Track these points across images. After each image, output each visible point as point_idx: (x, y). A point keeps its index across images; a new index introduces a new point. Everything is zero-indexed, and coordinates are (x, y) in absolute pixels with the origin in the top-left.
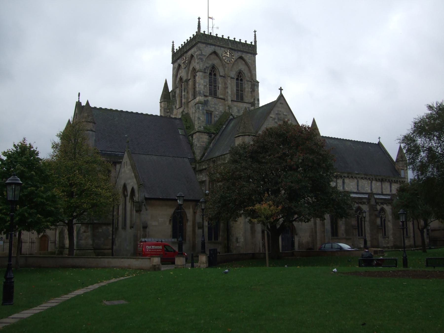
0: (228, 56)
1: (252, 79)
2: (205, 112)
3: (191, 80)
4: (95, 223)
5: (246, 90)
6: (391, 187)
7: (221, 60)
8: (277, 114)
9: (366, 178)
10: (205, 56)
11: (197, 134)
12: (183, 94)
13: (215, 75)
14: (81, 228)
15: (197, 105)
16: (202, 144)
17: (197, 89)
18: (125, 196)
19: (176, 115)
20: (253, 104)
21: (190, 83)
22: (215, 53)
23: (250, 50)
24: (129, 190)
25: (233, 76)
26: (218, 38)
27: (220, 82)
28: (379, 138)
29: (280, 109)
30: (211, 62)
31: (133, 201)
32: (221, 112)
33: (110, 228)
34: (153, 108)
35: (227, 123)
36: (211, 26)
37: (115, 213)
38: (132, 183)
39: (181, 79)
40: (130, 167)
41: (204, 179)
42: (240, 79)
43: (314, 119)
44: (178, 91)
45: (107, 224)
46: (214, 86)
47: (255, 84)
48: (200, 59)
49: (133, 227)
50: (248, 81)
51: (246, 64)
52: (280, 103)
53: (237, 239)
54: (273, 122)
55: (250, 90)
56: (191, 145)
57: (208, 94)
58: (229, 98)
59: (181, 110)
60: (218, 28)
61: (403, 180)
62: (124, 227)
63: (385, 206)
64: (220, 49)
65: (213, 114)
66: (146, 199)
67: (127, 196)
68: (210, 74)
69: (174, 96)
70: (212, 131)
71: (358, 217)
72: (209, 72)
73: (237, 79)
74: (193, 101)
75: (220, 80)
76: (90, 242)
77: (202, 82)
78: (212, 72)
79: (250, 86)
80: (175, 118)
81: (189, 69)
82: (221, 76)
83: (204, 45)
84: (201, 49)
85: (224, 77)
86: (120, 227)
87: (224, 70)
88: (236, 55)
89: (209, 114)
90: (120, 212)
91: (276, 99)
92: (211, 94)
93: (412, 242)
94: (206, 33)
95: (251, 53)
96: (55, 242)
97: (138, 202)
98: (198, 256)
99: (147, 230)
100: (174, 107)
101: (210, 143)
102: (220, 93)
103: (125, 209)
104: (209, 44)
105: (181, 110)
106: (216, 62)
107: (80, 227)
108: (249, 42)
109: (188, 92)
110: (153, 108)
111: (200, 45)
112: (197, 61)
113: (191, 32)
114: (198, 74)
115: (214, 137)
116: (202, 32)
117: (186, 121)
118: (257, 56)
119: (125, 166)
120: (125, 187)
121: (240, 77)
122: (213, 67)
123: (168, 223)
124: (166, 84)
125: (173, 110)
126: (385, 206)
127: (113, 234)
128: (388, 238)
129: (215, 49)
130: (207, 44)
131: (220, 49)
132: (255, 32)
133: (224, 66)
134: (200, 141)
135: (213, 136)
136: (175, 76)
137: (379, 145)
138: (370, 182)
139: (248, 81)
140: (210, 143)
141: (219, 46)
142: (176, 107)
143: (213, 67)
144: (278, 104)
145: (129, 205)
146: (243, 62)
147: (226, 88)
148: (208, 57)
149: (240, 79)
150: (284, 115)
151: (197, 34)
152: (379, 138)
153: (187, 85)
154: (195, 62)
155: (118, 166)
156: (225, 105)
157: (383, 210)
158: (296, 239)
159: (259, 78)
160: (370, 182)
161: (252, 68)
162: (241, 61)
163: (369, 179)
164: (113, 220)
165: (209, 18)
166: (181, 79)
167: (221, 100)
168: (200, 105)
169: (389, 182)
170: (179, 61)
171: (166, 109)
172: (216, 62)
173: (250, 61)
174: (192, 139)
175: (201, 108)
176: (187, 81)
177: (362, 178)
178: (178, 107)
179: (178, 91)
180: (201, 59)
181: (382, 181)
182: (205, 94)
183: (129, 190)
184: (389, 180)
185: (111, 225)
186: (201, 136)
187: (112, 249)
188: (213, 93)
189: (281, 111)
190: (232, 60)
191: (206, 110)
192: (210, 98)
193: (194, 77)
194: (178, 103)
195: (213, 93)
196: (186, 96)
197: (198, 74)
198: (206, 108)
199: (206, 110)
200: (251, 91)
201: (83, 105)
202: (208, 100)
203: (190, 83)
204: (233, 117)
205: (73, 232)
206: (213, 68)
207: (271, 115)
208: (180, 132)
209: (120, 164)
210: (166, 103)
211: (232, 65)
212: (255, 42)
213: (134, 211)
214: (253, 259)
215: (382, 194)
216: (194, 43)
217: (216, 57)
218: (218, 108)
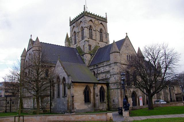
5: (104, 37)
20: (107, 43)
22: (91, 20)
24: (61, 78)
30: (90, 24)
34: (61, 42)
39: (75, 32)
43: (37, 38)
44: (73, 37)
45: (48, 96)
47: (107, 35)
53: (114, 100)
58: (98, 41)
65: (92, 46)
66: (72, 82)
69: (71, 40)
70: (92, 53)
78: (90, 28)
89: (90, 46)
91: (113, 43)
92: (90, 38)
101: (91, 58)
102: (94, 37)
108: (104, 17)
111: (85, 16)
113: (82, 11)
120: (58, 78)
122: (91, 26)
124: (67, 34)
127: (51, 101)
132: (106, 13)
136: (71, 31)
143: (91, 26)
144: (126, 40)
159: (109, 31)
161: (105, 28)
166: (75, 32)
168: (87, 42)
183: (61, 78)
185: (50, 97)
187: (51, 108)
188: (91, 37)
192: (90, 39)
195: (91, 37)
208: (77, 54)
212: (106, 17)
218: (93, 44)
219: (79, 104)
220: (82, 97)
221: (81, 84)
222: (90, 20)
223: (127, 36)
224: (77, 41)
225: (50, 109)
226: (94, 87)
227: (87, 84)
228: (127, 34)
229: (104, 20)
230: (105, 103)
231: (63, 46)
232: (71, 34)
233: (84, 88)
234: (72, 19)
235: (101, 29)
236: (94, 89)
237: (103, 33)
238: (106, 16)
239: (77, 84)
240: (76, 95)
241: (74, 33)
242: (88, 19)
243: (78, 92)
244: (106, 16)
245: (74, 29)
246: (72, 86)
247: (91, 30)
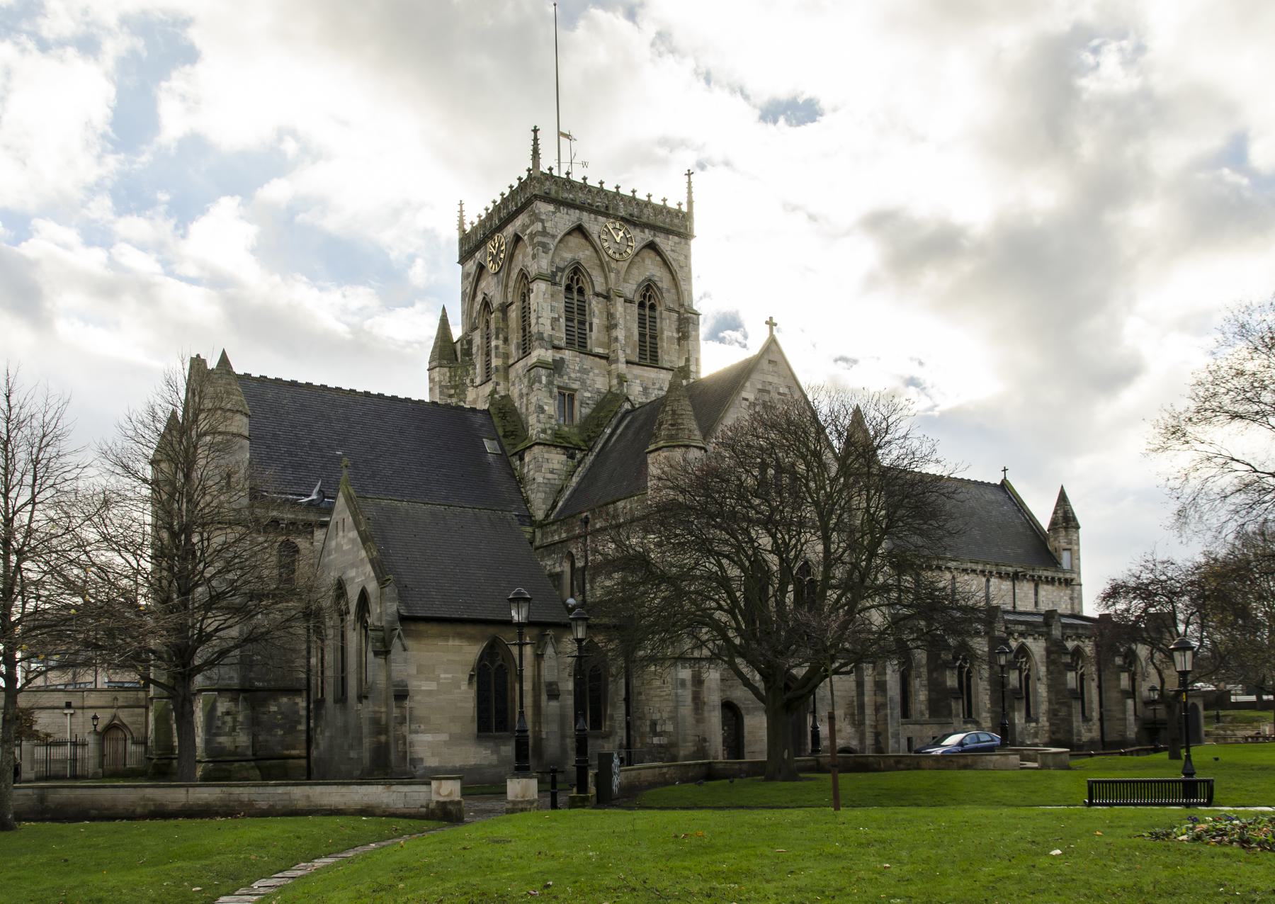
0: (618, 239)
1: (682, 305)
2: (556, 390)
3: (514, 307)
4: (258, 690)
5: (666, 334)
6: (1036, 594)
7: (596, 251)
8: (760, 391)
9: (974, 571)
10: (553, 236)
11: (536, 449)
12: (493, 343)
13: (581, 291)
14: (218, 704)
15: (533, 372)
16: (550, 476)
17: (534, 329)
18: (343, 614)
19: (475, 401)
21: (514, 314)
24: (353, 594)
25: (630, 296)
27: (597, 312)
28: (1005, 470)
29: (770, 378)
30: (568, 256)
31: (366, 628)
32: (599, 392)
33: (301, 702)
34: (414, 384)
35: (614, 422)
36: (565, 157)
37: (313, 661)
38: (361, 576)
39: (486, 304)
40: (354, 534)
41: (558, 569)
42: (648, 304)
43: (224, 353)
44: (477, 339)
45: (292, 691)
46: (579, 322)
47: (686, 321)
48: (540, 244)
49: (366, 697)
50: (670, 310)
51: (666, 263)
55: (676, 335)
56: (519, 482)
57: (563, 344)
58: (622, 359)
59: (488, 388)
60: (585, 164)
61: (1068, 576)
62: (342, 699)
63: (1029, 642)
64: (596, 220)
65: (577, 396)
67: (348, 612)
68: (569, 288)
69: (468, 352)
70: (576, 440)
71: (961, 667)
72: (564, 282)
73: (641, 305)
74: (521, 363)
75: (596, 305)
76: (243, 739)
77: (546, 306)
78: (574, 283)
79: (674, 326)
80: (473, 410)
81: (508, 275)
82: (598, 295)
83: (551, 208)
84: (543, 217)
85: (605, 297)
86: (330, 698)
87: (606, 278)
88: (638, 238)
89: (567, 398)
90: (329, 658)
92: (570, 344)
93: (1095, 734)
95: (679, 234)
96: (145, 743)
97: (381, 629)
99: (407, 703)
100: (468, 381)
102: (595, 337)
103: (343, 649)
105: (488, 388)
106: (584, 254)
107: (215, 701)
108: (672, 204)
109: (506, 340)
112: (529, 249)
114: (534, 286)
115: (583, 458)
116: (544, 168)
117: (504, 417)
118: (693, 243)
119: (341, 533)
120: (340, 587)
121: (648, 299)
123: (464, 686)
125: (464, 392)
126: (1029, 642)
128: (1037, 721)
129: (580, 219)
130: (559, 203)
131: (596, 220)
134: (545, 469)
135: (579, 455)
136: (469, 296)
138: (984, 580)
139: (670, 310)
140: (571, 474)
142: (472, 381)
145: (353, 638)
146: (658, 258)
147: (611, 326)
148: (561, 241)
149: (648, 304)
150: (779, 394)
151: (530, 175)
152: (1005, 470)
153: (505, 317)
154: (524, 256)
155: (319, 534)
156: (609, 373)
157: (1023, 651)
160: (984, 580)
161: (676, 274)
162: (652, 254)
163: (983, 572)
164: (308, 680)
165: (560, 134)
166: (486, 304)
167: (597, 359)
168: (543, 372)
169: (1034, 580)
170: (478, 255)
171: (447, 387)
172: (584, 254)
173: (674, 255)
174: (522, 466)
176: (504, 308)
177: (965, 570)
178: (478, 381)
179: (477, 339)
180: (544, 246)
181: (1015, 577)
182: (556, 342)
183: (353, 594)
184: (1032, 576)
185: (305, 694)
186: (546, 456)
187: (308, 757)
189: (770, 383)
190: (629, 250)
191: (559, 387)
192: (567, 354)
193: (525, 296)
194: (478, 371)
195: (578, 341)
196: (501, 350)
197: (534, 286)
199: (559, 387)
200: (679, 339)
201: (209, 367)
202: (562, 359)
203: (514, 314)
204: (632, 405)
205: (192, 713)
206: (575, 274)
207: (744, 394)
208: (489, 445)
209: (324, 530)
210: (446, 370)
211: (626, 264)
212: (690, 203)
213: (371, 655)
214: (712, 777)
215: (1014, 612)
216: (521, 199)
217: (583, 241)
218: (594, 381)
219: (444, 737)
220: (465, 697)
221: (460, 629)
222: (569, 226)
223: (772, 346)
224: (495, 362)
225: (304, 762)
227: (491, 630)
228: (771, 323)
229: (662, 228)
231: (415, 398)
232: (467, 314)
233: (470, 652)
234: (476, 212)
235: (649, 288)
236: (539, 657)
237: (661, 312)
238: (690, 193)
239: (433, 629)
240: (421, 686)
241: (481, 310)
242: (563, 220)
243: (439, 674)
244: (690, 193)
245: (483, 284)
246: (396, 641)
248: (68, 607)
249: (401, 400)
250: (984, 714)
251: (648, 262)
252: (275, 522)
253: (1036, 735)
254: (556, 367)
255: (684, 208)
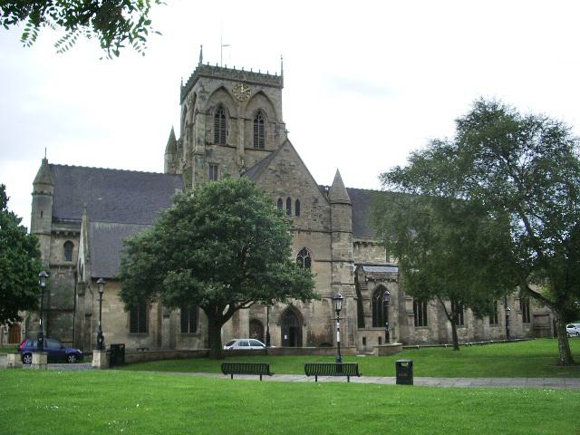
22: (222, 88)
23: (276, 82)
26: (245, 72)
30: (217, 101)
34: (155, 163)
43: (338, 173)
51: (268, 100)
52: (285, 150)
54: (274, 175)
65: (219, 167)
68: (217, 116)
69: (181, 146)
75: (229, 122)
83: (208, 80)
92: (216, 142)
94: (219, 66)
95: (275, 87)
98: (92, 354)
102: (229, 140)
104: (212, 78)
106: (224, 100)
110: (155, 163)
116: (205, 63)
118: (283, 90)
121: (259, 117)
122: (221, 107)
124: (173, 130)
133: (236, 105)
137: (6, 200)
141: (228, 80)
143: (221, 107)
147: (237, 133)
148: (213, 94)
158: (305, 331)
161: (275, 106)
175: (199, 160)
188: (220, 138)
192: (214, 147)
198: (208, 160)
207: (270, 167)
226: (331, 331)
230: (199, 336)
247: (223, 117)
248: (185, 235)
249: (112, 170)
250: (434, 324)
251: (259, 100)
252: (62, 233)
253: (466, 334)
254: (208, 153)
255: (279, 75)
